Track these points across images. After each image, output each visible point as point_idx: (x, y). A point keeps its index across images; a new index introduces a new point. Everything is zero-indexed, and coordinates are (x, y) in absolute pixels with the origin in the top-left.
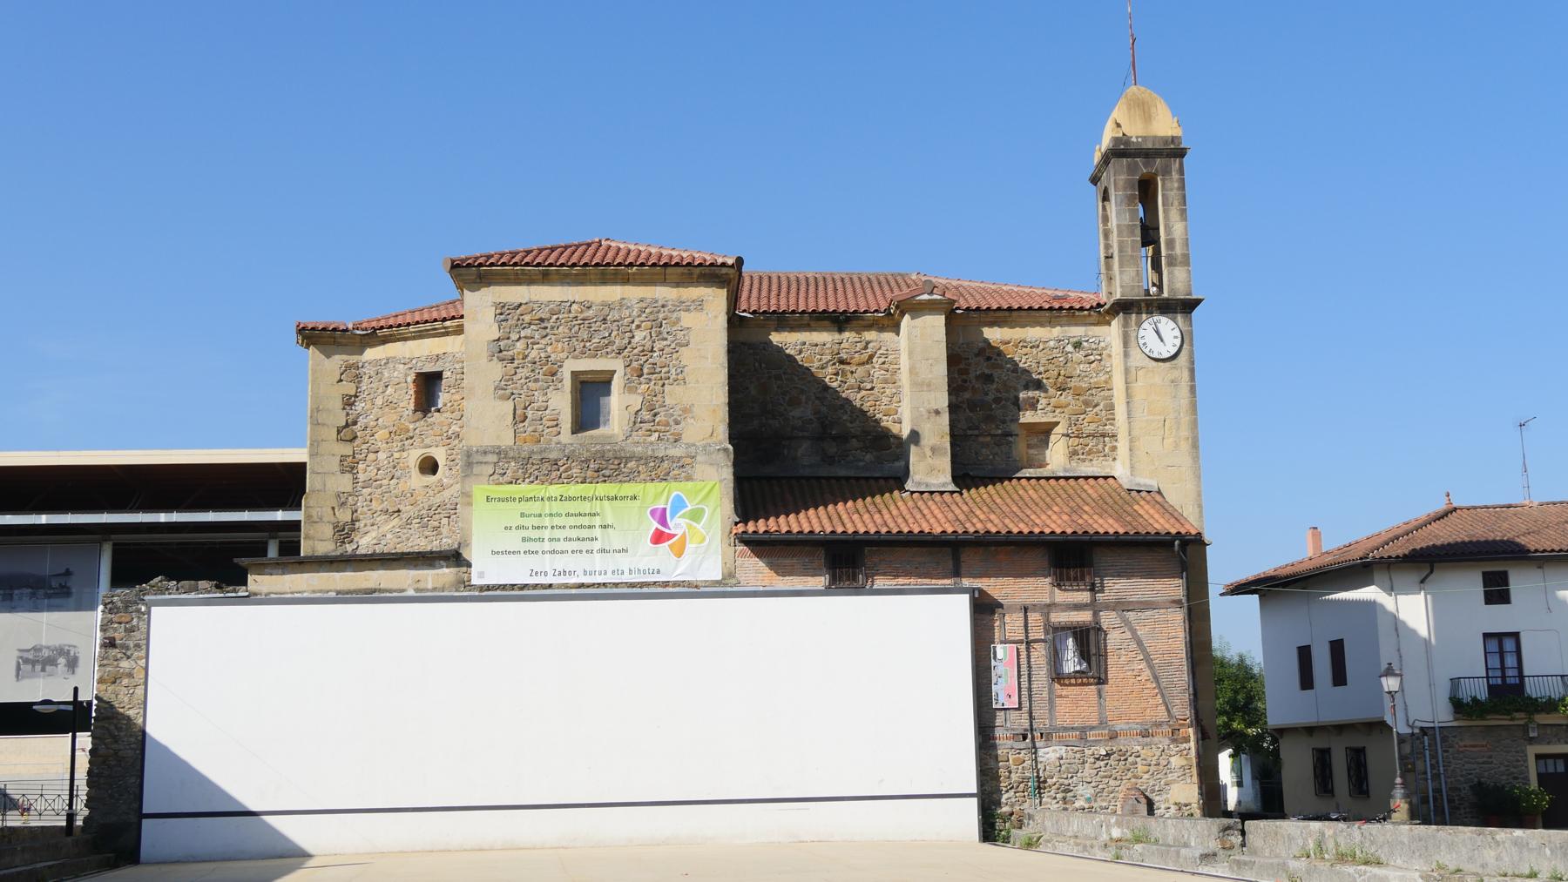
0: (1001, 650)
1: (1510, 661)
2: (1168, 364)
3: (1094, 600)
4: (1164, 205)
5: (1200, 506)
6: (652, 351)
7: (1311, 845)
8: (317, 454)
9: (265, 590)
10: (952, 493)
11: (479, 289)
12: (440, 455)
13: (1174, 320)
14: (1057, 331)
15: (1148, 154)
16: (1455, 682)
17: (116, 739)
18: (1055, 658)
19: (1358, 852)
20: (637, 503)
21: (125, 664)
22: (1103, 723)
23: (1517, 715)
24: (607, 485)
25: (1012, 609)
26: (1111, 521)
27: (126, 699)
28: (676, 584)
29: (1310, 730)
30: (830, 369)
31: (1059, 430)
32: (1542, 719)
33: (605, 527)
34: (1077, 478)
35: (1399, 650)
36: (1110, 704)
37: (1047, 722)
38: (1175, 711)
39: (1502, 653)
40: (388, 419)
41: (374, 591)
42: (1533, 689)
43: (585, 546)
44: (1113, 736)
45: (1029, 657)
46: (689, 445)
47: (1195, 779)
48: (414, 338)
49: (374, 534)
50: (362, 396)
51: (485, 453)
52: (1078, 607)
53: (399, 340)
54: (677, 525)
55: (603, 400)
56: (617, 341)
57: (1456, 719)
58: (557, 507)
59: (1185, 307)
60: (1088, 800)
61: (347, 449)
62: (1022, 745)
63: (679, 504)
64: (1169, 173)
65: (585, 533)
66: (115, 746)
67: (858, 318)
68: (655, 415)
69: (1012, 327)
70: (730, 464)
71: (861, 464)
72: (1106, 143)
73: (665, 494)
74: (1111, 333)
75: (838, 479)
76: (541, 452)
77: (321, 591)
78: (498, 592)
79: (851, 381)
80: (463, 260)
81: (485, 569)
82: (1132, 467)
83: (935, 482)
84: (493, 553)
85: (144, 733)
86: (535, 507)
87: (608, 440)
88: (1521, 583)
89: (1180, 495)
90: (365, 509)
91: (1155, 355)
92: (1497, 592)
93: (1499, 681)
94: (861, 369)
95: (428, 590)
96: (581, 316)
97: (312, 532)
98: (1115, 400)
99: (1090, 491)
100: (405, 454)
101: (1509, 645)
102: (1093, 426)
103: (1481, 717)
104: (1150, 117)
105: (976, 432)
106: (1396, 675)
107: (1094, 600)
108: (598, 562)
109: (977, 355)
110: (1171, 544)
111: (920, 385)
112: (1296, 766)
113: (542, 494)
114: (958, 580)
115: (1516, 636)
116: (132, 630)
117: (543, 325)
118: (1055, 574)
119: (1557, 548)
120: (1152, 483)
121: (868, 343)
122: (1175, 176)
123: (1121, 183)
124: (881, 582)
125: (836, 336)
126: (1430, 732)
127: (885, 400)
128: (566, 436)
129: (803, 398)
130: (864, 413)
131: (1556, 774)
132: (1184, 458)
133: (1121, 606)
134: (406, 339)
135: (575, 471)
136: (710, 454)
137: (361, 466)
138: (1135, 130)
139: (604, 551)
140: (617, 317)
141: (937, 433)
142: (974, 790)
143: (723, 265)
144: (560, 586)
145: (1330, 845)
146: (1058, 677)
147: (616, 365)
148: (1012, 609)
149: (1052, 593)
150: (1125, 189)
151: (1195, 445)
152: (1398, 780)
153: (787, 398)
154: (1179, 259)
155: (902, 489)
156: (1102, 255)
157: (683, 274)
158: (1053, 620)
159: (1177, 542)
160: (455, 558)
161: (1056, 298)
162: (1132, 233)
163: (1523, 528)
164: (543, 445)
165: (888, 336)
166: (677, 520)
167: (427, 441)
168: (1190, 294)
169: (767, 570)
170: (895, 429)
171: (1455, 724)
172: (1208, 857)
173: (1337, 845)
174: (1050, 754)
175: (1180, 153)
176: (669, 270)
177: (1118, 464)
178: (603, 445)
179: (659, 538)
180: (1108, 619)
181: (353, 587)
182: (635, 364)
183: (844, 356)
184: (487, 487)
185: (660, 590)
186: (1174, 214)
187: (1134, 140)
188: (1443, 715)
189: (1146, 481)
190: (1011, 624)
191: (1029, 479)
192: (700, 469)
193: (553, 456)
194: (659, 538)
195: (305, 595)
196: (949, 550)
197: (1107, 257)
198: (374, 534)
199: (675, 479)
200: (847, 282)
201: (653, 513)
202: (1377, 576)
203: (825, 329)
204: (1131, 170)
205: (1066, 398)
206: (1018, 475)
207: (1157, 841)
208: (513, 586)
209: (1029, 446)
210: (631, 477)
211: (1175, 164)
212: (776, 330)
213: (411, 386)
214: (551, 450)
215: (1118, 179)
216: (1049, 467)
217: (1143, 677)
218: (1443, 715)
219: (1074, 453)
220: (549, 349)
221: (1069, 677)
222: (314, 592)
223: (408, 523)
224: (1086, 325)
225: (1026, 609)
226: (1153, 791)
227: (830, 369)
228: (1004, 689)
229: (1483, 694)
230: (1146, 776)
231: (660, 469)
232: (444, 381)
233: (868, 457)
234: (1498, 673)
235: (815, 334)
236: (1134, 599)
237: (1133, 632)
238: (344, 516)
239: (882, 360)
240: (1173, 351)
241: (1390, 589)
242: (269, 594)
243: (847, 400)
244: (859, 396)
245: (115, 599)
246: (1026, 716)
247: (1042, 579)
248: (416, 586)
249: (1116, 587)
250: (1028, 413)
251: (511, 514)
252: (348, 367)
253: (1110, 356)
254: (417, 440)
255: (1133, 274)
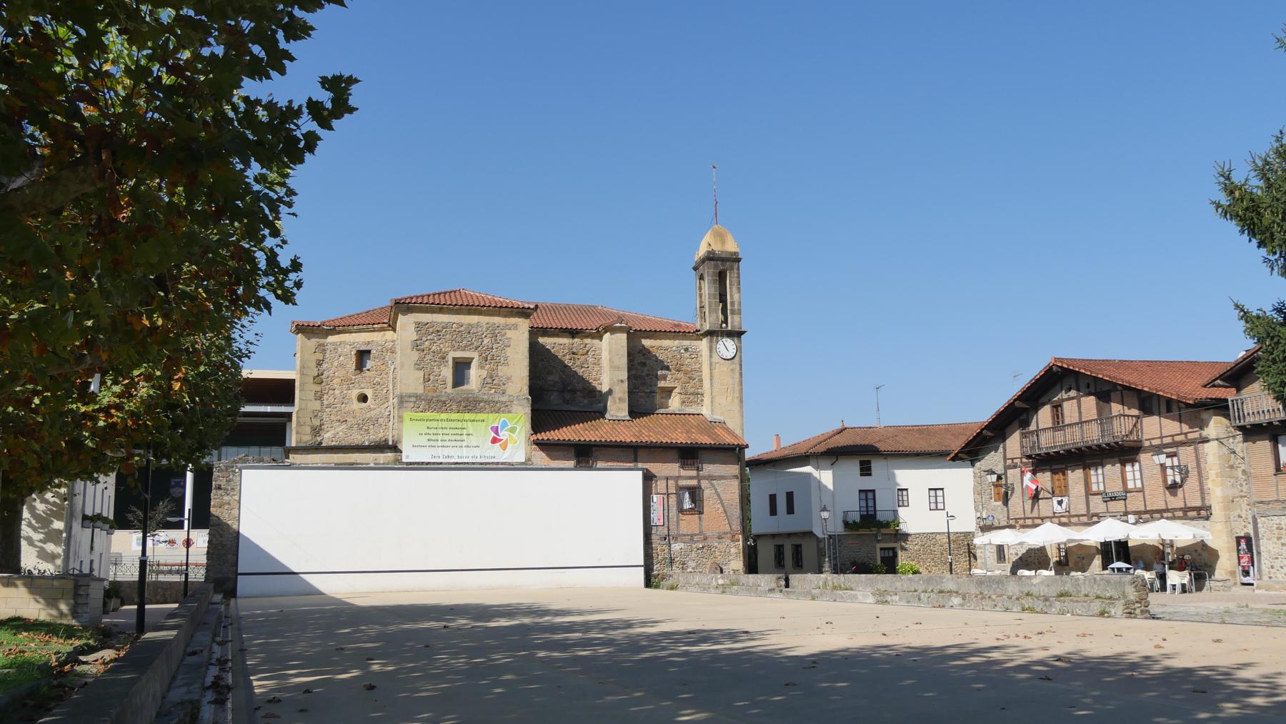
0: (655, 498)
1: (871, 503)
2: (730, 362)
3: (698, 474)
4: (730, 285)
5: (743, 430)
6: (492, 349)
7: (821, 583)
8: (303, 390)
9: (298, 462)
10: (629, 421)
11: (406, 315)
12: (369, 393)
13: (733, 340)
14: (677, 342)
15: (723, 260)
16: (846, 513)
17: (221, 536)
18: (680, 502)
19: (842, 585)
20: (484, 423)
21: (226, 498)
22: (701, 533)
23: (873, 529)
24: (469, 414)
25: (661, 478)
26: (706, 437)
27: (227, 516)
28: (503, 463)
29: (774, 536)
30: (568, 357)
31: (676, 390)
32: (884, 531)
33: (469, 435)
34: (685, 414)
35: (820, 497)
36: (704, 523)
37: (676, 532)
38: (733, 527)
39: (867, 499)
40: (339, 374)
41: (354, 464)
42: (880, 517)
43: (459, 444)
44: (705, 539)
45: (668, 501)
46: (510, 396)
47: (742, 558)
48: (356, 332)
49: (332, 432)
50: (326, 360)
51: (410, 397)
52: (691, 478)
53: (347, 333)
54: (503, 435)
55: (466, 371)
56: (475, 343)
57: (845, 531)
58: (445, 424)
59: (737, 334)
60: (693, 568)
61: (318, 388)
62: (664, 542)
63: (505, 424)
64: (733, 269)
65: (459, 438)
66: (221, 539)
67: (582, 332)
68: (493, 380)
69: (656, 340)
70: (530, 405)
71: (582, 404)
72: (702, 251)
73: (498, 420)
74: (703, 344)
75: (571, 411)
76: (437, 397)
77: (327, 463)
78: (416, 466)
79: (578, 363)
80: (401, 300)
81: (409, 454)
82: (712, 410)
83: (621, 415)
84: (413, 446)
85: (238, 532)
86: (434, 424)
87: (470, 392)
88: (877, 466)
89: (733, 424)
90: (328, 419)
91: (724, 357)
92: (866, 470)
93: (865, 513)
94: (582, 357)
95: (380, 464)
96: (457, 330)
97: (300, 430)
98: (703, 377)
99: (693, 421)
100: (350, 392)
101: (870, 496)
102: (693, 389)
103: (857, 530)
104: (724, 242)
105: (637, 391)
106: (828, 511)
107: (698, 474)
108: (465, 452)
109: (639, 353)
110: (735, 449)
111: (614, 367)
112: (766, 553)
113: (438, 418)
114: (635, 464)
115: (873, 491)
116: (230, 481)
117: (439, 334)
118: (681, 462)
119: (894, 450)
120: (722, 418)
121: (586, 344)
122: (735, 271)
123: (710, 273)
124: (600, 464)
125: (571, 340)
126: (833, 537)
127: (594, 373)
128: (449, 389)
129: (554, 371)
130: (584, 379)
131: (252, 688)
132: (736, 407)
133: (711, 478)
134: (351, 332)
135: (454, 407)
136: (520, 400)
137: (325, 397)
138: (717, 248)
139: (468, 446)
140: (475, 331)
141: (621, 391)
142: (643, 564)
143: (529, 308)
144: (446, 463)
145: (830, 583)
146: (681, 510)
147: (475, 355)
148: (661, 478)
149: (679, 471)
150: (712, 276)
151: (741, 401)
152: (827, 559)
153: (546, 370)
154: (737, 311)
155: (604, 417)
156: (698, 306)
157: (508, 312)
158: (679, 484)
159: (737, 449)
160: (395, 448)
161: (676, 326)
162: (715, 298)
163: (877, 439)
164: (438, 393)
165: (596, 341)
166: (504, 432)
167: (362, 385)
168: (741, 328)
169: (546, 457)
170: (598, 388)
171: (845, 533)
172: (771, 590)
173: (833, 583)
174: (676, 547)
175: (738, 260)
176: (502, 309)
177: (704, 408)
178: (468, 394)
179: (495, 441)
180: (704, 484)
181: (343, 462)
182: (484, 355)
183: (575, 350)
184: (410, 413)
185: (495, 466)
186: (735, 289)
187: (717, 252)
188: (839, 529)
189: (718, 417)
190: (660, 486)
191: (662, 414)
192: (515, 408)
193: (443, 399)
194: (495, 441)
195: (319, 465)
196: (632, 449)
197: (701, 307)
198: (332, 432)
199: (503, 412)
200: (568, 309)
201: (492, 428)
202: (811, 462)
203: (566, 337)
204: (716, 267)
205: (680, 375)
206: (657, 412)
207: (743, 585)
208: (423, 463)
209: (662, 398)
210: (481, 411)
211: (736, 265)
212: (541, 336)
213: (354, 356)
214: (442, 396)
215: (708, 271)
216: (670, 408)
217: (720, 511)
218: (839, 529)
219: (684, 402)
220: (441, 346)
221: (686, 510)
222: (323, 464)
223: (351, 427)
224: (690, 340)
225: (667, 479)
226: (723, 564)
227: (568, 357)
228: (657, 517)
229: (858, 520)
230: (719, 557)
231: (496, 407)
232: (371, 355)
233: (586, 401)
234: (865, 509)
235: (561, 339)
236: (716, 474)
237: (716, 490)
238: (316, 422)
239: (593, 353)
240: (733, 355)
241: (817, 468)
242: (301, 464)
243: (575, 372)
244: (582, 371)
245: (221, 465)
246: (666, 529)
247: (675, 464)
248: (375, 462)
249: (709, 469)
250: (662, 382)
251: (422, 427)
252: (320, 345)
253: (701, 356)
254: (357, 385)
255: (715, 317)
